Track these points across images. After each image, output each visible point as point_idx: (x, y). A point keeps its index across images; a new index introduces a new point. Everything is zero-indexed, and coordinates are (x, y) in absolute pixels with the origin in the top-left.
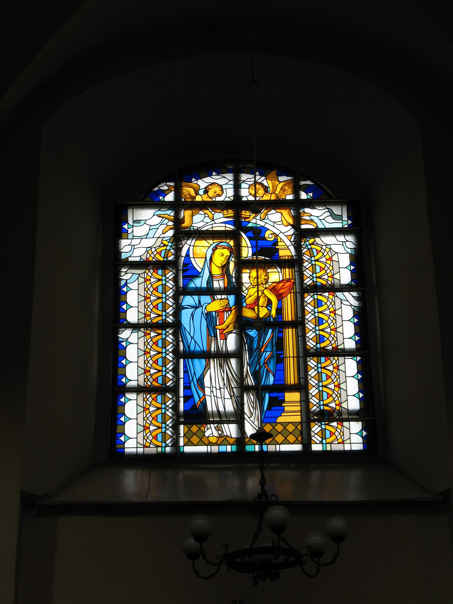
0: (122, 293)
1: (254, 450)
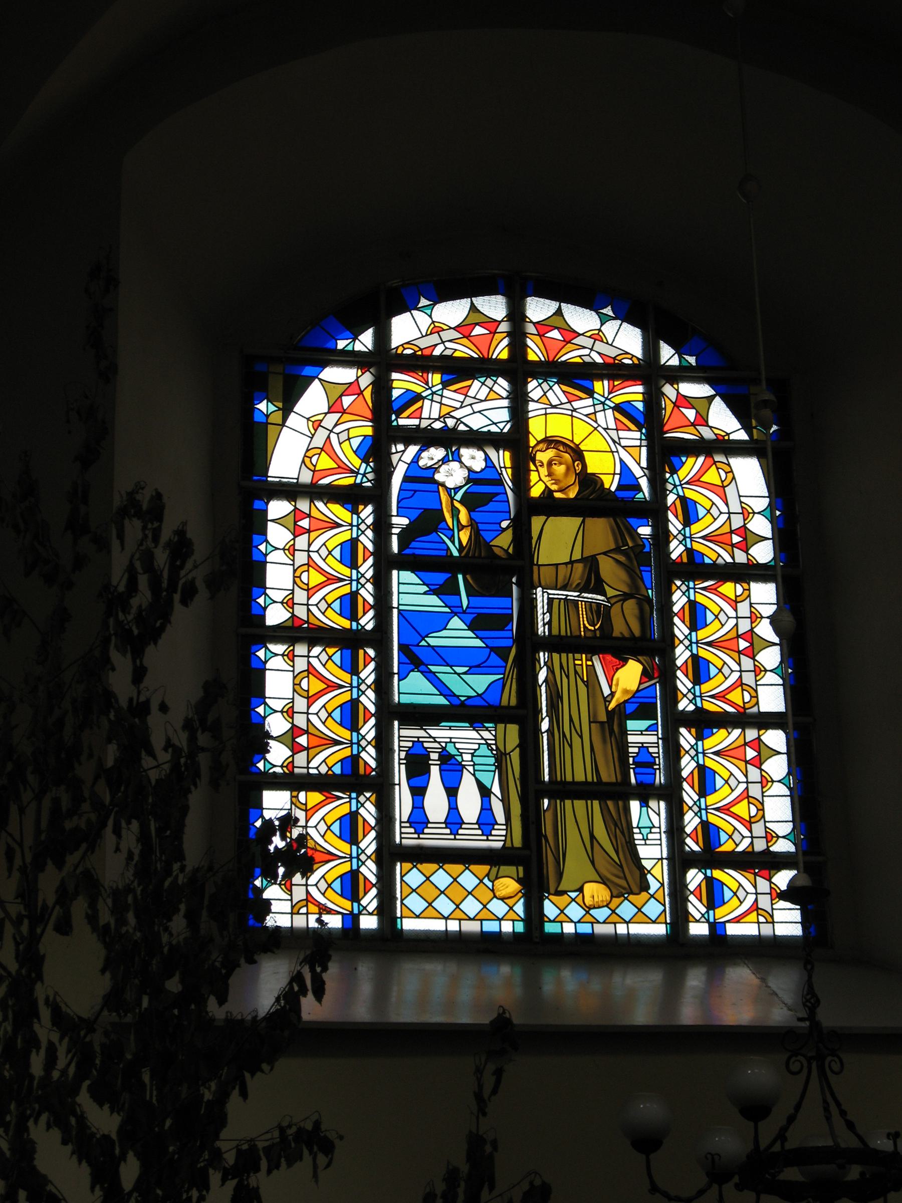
1: (560, 931)
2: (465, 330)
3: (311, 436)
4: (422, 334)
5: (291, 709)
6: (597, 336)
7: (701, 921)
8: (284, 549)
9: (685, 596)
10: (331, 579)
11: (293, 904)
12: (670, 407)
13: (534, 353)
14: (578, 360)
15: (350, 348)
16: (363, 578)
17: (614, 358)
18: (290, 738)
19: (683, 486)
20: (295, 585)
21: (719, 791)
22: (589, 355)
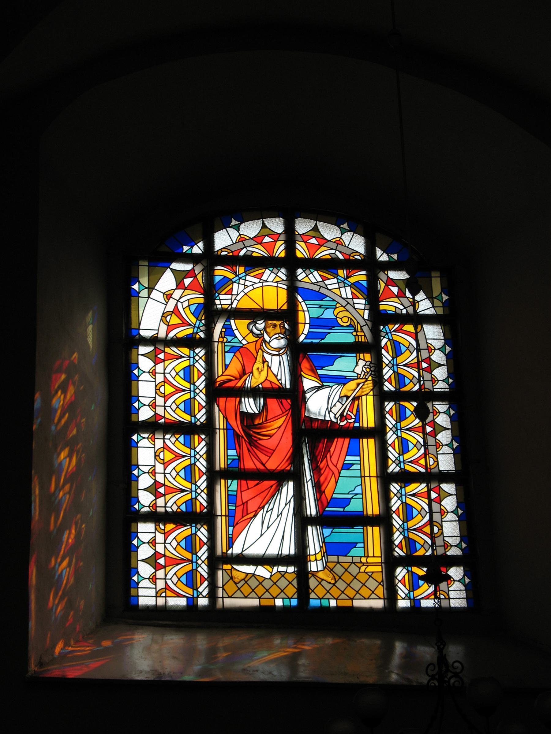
0: (133, 293)
2: (258, 240)
3: (166, 303)
4: (233, 242)
5: (155, 505)
6: (339, 242)
7: (405, 598)
8: (149, 372)
9: (392, 370)
10: (178, 390)
11: (157, 591)
12: (383, 285)
13: (301, 251)
14: (329, 257)
15: (189, 252)
16: (197, 356)
17: (350, 255)
18: (154, 489)
19: (392, 333)
20: (156, 394)
21: (408, 419)
22: (335, 253)
